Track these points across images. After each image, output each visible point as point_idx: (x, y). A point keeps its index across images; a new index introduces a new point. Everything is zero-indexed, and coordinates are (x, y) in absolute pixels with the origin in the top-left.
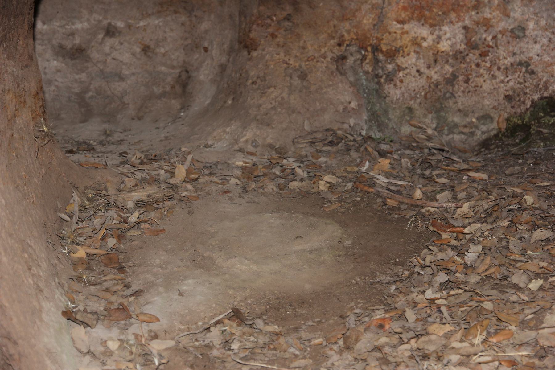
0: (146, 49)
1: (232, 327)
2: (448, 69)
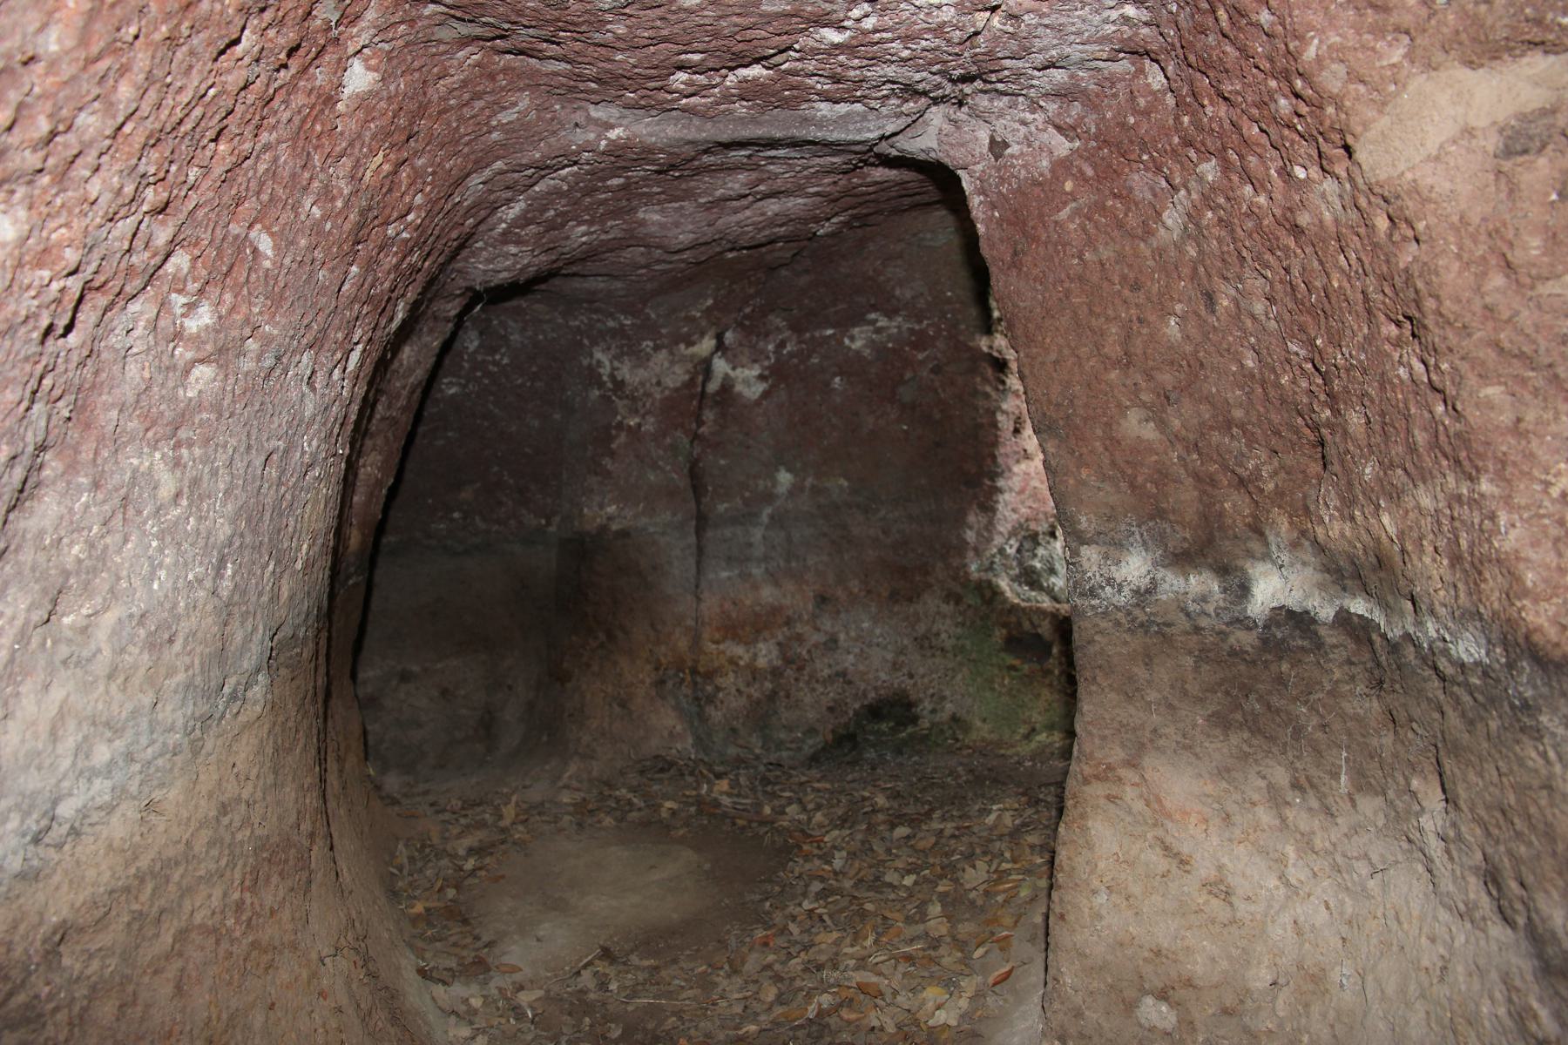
0: (445, 692)
1: (602, 967)
2: (768, 685)
